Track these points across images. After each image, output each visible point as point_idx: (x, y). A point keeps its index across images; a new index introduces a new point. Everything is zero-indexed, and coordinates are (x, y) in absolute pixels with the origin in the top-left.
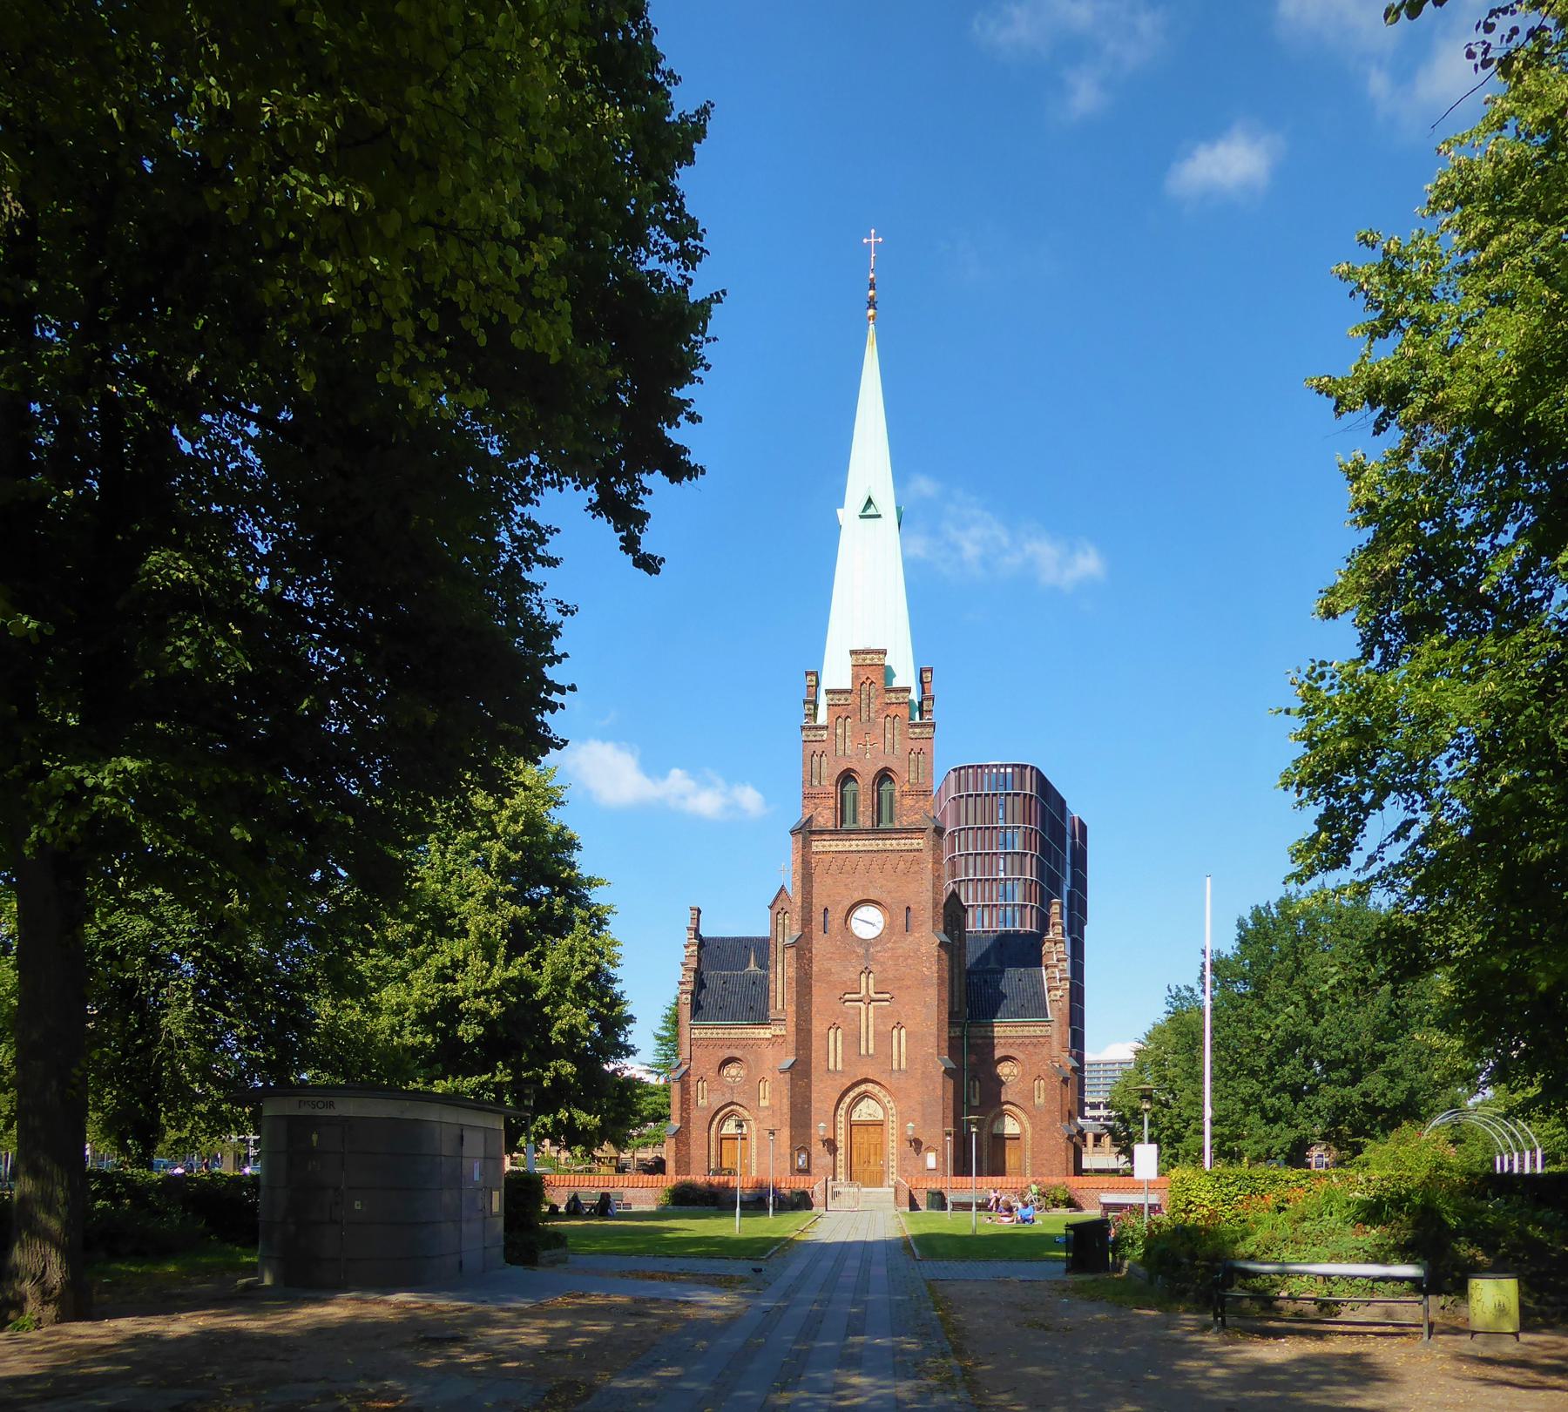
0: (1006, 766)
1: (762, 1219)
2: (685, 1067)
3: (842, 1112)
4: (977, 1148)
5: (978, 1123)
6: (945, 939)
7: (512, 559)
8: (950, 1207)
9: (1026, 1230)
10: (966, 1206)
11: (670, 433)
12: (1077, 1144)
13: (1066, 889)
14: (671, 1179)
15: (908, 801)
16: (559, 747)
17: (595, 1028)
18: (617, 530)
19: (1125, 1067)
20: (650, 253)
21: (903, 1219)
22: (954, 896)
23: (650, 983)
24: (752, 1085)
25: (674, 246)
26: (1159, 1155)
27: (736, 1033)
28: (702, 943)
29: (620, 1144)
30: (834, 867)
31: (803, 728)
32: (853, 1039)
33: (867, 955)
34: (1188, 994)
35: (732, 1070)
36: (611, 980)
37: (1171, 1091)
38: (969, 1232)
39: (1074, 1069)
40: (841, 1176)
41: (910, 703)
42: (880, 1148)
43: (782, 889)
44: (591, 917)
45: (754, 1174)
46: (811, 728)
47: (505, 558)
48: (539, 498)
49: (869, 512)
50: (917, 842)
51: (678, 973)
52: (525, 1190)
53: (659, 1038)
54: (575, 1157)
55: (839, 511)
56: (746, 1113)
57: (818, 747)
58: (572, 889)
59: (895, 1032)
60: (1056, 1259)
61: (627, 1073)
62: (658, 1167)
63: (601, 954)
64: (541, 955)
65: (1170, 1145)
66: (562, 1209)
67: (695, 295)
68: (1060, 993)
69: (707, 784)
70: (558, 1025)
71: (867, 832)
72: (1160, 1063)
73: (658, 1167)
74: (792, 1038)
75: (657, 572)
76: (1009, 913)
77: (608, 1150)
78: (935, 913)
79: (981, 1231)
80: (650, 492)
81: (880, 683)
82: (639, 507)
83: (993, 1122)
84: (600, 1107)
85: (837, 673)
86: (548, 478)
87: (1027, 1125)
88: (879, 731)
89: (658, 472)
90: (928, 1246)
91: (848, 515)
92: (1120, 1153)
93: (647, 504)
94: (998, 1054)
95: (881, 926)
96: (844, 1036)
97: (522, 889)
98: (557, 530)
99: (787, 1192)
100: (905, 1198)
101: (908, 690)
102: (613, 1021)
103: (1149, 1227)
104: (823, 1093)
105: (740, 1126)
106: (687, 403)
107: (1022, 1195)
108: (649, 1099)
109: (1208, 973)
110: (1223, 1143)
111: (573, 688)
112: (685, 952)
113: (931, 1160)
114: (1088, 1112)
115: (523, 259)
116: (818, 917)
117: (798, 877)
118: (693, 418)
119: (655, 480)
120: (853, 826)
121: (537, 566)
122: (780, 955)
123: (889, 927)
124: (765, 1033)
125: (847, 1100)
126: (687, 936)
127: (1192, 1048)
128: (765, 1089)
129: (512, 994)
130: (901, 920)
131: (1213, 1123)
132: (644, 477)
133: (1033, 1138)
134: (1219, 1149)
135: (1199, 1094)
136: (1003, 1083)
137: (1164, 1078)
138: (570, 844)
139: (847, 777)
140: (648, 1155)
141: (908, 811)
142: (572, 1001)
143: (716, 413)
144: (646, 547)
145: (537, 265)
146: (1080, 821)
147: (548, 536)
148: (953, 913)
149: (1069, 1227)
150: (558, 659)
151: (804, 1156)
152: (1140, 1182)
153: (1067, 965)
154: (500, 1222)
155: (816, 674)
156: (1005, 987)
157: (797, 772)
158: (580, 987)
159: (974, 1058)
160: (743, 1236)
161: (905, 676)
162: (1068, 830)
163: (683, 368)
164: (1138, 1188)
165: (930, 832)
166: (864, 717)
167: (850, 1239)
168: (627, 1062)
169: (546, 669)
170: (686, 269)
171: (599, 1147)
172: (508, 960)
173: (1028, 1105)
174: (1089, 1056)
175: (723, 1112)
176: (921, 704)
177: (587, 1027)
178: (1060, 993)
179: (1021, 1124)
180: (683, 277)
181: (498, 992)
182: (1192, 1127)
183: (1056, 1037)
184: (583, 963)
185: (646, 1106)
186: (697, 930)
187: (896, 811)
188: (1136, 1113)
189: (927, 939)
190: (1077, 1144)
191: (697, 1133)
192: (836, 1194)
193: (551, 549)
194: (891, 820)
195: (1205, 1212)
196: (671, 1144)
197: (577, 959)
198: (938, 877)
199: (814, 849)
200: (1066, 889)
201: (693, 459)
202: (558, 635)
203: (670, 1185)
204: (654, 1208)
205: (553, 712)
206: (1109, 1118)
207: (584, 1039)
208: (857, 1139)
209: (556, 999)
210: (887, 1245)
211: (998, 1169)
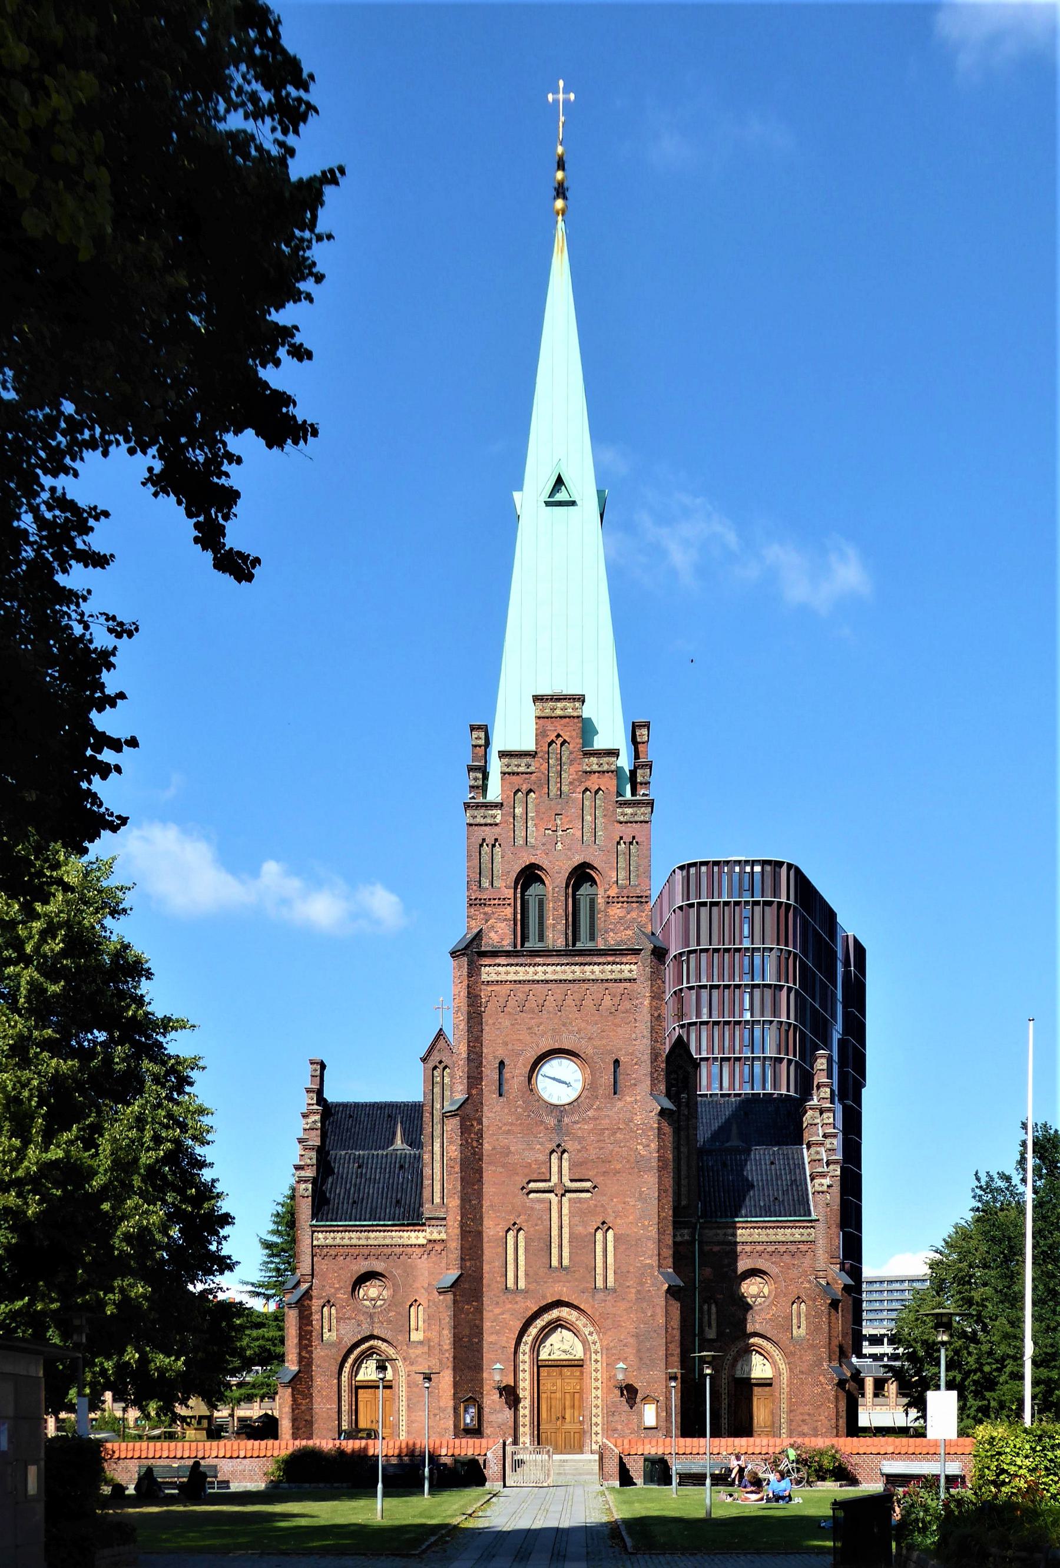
0: (753, 863)
1: (414, 1500)
2: (304, 1286)
3: (525, 1348)
4: (715, 1401)
5: (713, 1362)
6: (668, 1104)
7: (39, 554)
8: (675, 1480)
9: (781, 1510)
10: (697, 1479)
11: (268, 374)
12: (850, 1392)
13: (836, 1035)
14: (286, 1445)
15: (616, 911)
16: (115, 829)
17: (175, 1232)
18: (190, 515)
19: (918, 1285)
20: (232, 106)
21: (611, 1498)
22: (680, 1046)
23: (254, 1170)
24: (400, 1311)
25: (266, 97)
26: (962, 1409)
27: (376, 1238)
28: (328, 1111)
29: (213, 1396)
30: (512, 1003)
31: (467, 806)
32: (541, 1246)
33: (559, 1128)
34: (1002, 1184)
35: (372, 1290)
36: (202, 1165)
37: (979, 1319)
38: (701, 1514)
39: (846, 1288)
40: (525, 1439)
41: (618, 771)
42: (578, 1399)
43: (440, 1034)
44: (168, 1073)
45: (403, 1436)
46: (478, 806)
47: (28, 553)
48: (77, 465)
49: (562, 496)
50: (628, 969)
51: (294, 1153)
52: (81, 1458)
53: (267, 1245)
54: (147, 1417)
55: (517, 495)
56: (391, 1351)
57: (489, 834)
58: (143, 1033)
59: (599, 1235)
60: (822, 1550)
61: (221, 1296)
62: (267, 1428)
63: (184, 1127)
64: (97, 1129)
65: (977, 1394)
66: (131, 1490)
67: (299, 170)
68: (827, 1181)
69: (315, 883)
70: (124, 1227)
71: (559, 953)
72: (964, 1280)
73: (267, 1428)
74: (455, 1245)
75: (250, 578)
76: (758, 1069)
77: (196, 1406)
78: (654, 1069)
79: (718, 1513)
80: (239, 461)
81: (575, 744)
82: (223, 481)
83: (735, 1361)
84: (183, 1343)
85: (515, 728)
86: (87, 434)
87: (783, 1366)
88: (574, 811)
89: (249, 432)
90: (641, 1533)
91: (529, 499)
92: (909, 1405)
93: (235, 477)
94: (743, 1265)
95: (578, 1086)
96: (527, 1240)
97: (67, 1036)
98: (106, 514)
99: (445, 1460)
100: (613, 1468)
101: (614, 753)
102: (203, 1220)
103: (946, 1506)
104: (499, 1322)
105: (381, 1368)
106: (287, 332)
107: (776, 1463)
108: (255, 1333)
109: (1030, 1155)
110: (1050, 1392)
111: (133, 743)
112: (302, 1123)
113: (650, 1415)
114: (867, 1349)
115: (35, 102)
116: (490, 1073)
117: (463, 1017)
118: (301, 353)
119: (245, 443)
120: (539, 946)
121: (77, 567)
122: (438, 1128)
123: (591, 1087)
124: (416, 1237)
125: (533, 1331)
126: (306, 1101)
127: (1007, 1260)
128: (418, 1317)
129: (57, 1185)
130: (607, 1078)
131: (1034, 1363)
132: (229, 438)
133: (790, 1383)
134: (1045, 1399)
135: (1017, 1323)
136: (749, 1307)
137: (969, 1302)
138: (137, 969)
139: (530, 876)
140: (253, 1411)
141: (617, 925)
142: (142, 1194)
143: (332, 342)
144: (236, 536)
145: (56, 112)
146: (856, 940)
147: (91, 522)
148: (678, 1069)
149: (837, 1505)
150: (111, 701)
151: (472, 1410)
152: (936, 1443)
153: (837, 1143)
154: (40, 1508)
155: (485, 729)
156: (751, 1172)
157: (459, 870)
158: (152, 1172)
159: (708, 1271)
160: (387, 1522)
161: (611, 734)
162: (840, 954)
163: (289, 277)
164: (930, 1455)
165: (646, 954)
166: (554, 791)
167: (538, 1525)
168: (225, 1280)
169: (94, 715)
170: (285, 132)
171: (184, 1402)
172: (49, 1137)
173: (783, 1338)
174: (869, 1270)
175: (361, 1348)
176: (633, 773)
177: (164, 1229)
178: (827, 1181)
179: (774, 1364)
180: (281, 144)
181: (36, 1182)
182: (1008, 1370)
183: (821, 1242)
184: (157, 1140)
185: (249, 1342)
186: (320, 1092)
187: (600, 924)
188: (932, 1348)
189: (643, 1105)
190: (850, 1392)
191: (322, 1382)
192: (518, 1464)
193: (98, 540)
194: (592, 938)
195: (1023, 1485)
196: (285, 1396)
197: (148, 1134)
198: (657, 1019)
199: (484, 977)
200: (836, 1035)
201: (301, 413)
202: (110, 666)
203: (285, 1453)
204: (262, 1486)
205: (104, 777)
206: (895, 1357)
207: (160, 1248)
208: (546, 1385)
209: (118, 1190)
210: (588, 1532)
211: (743, 1427)
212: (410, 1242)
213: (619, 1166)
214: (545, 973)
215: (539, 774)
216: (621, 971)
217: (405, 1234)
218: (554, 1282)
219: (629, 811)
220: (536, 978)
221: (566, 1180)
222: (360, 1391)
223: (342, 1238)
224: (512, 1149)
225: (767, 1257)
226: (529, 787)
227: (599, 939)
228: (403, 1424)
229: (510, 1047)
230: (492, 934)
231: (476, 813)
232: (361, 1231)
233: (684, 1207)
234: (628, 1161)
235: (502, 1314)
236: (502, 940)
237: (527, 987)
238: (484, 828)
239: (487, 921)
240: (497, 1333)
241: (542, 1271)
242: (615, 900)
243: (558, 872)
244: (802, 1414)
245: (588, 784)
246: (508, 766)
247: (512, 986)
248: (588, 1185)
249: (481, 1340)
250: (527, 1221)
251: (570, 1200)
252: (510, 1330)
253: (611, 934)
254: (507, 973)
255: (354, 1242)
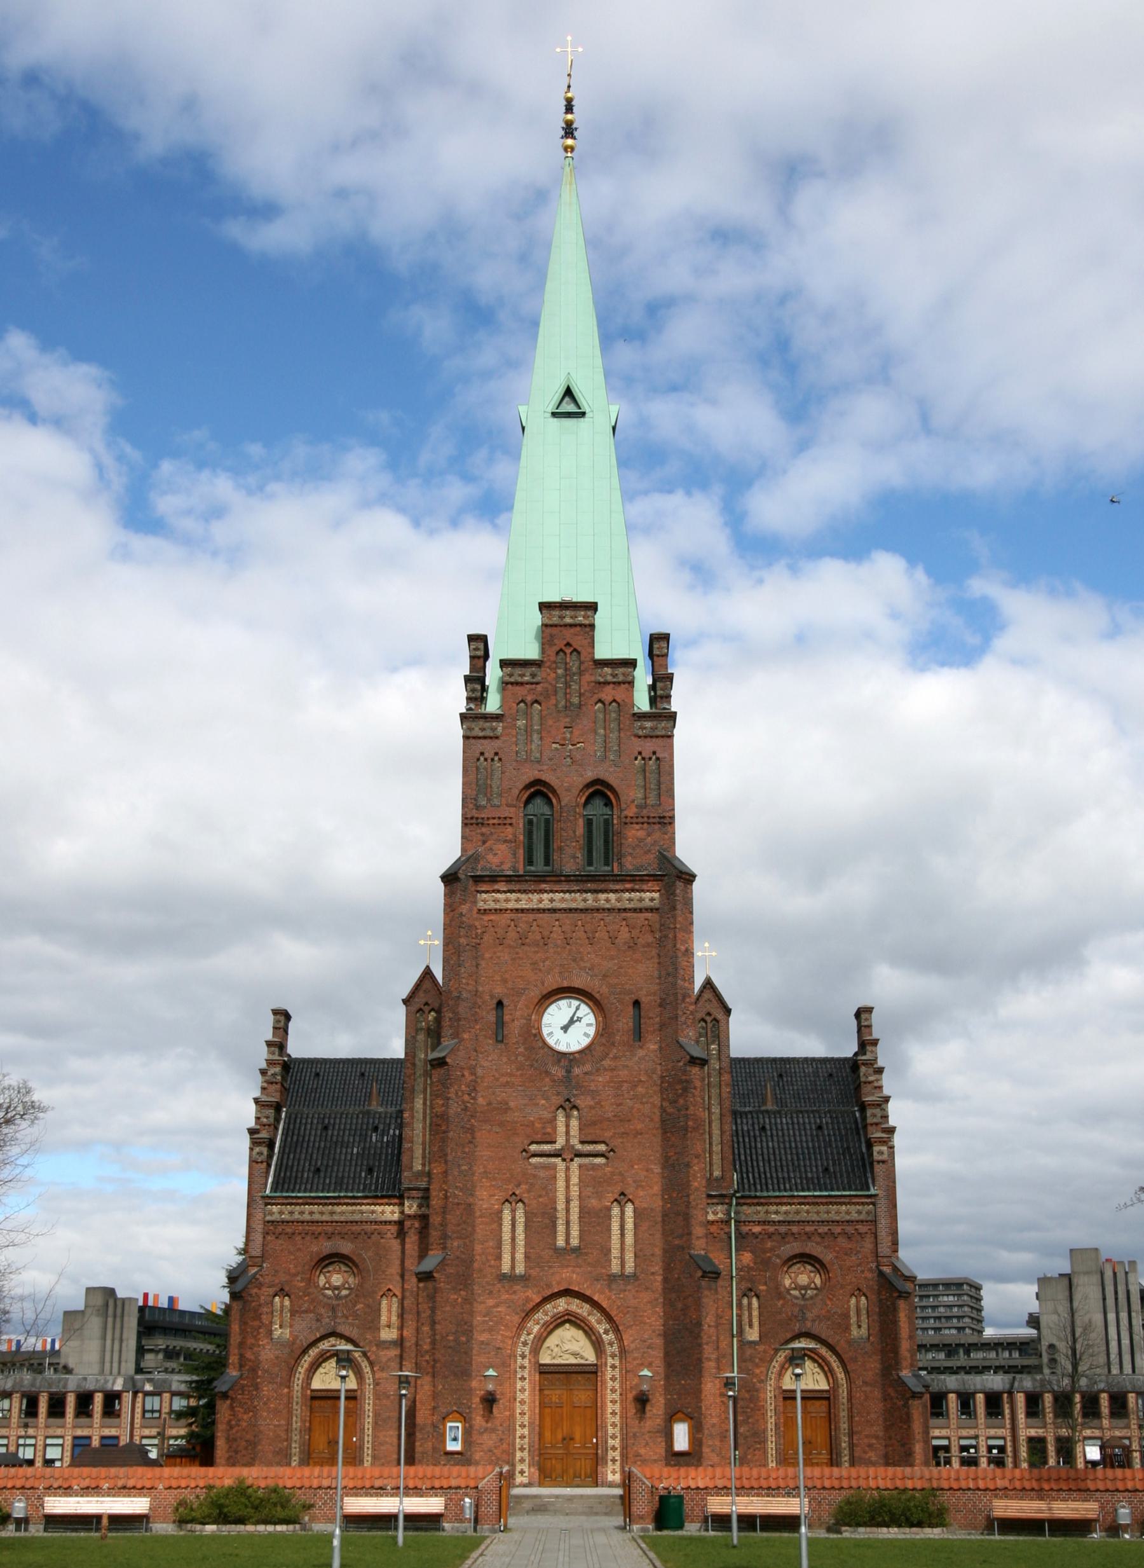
27: (343, 1212)
30: (512, 934)
32: (542, 1223)
33: (568, 1080)
49: (569, 407)
57: (489, 747)
87: (841, 1375)
123: (604, 1032)
212: (383, 1218)
213: (639, 1126)
214: (552, 900)
215: (546, 685)
216: (641, 900)
217: (379, 1208)
218: (563, 1266)
219: (648, 724)
220: (541, 906)
221: (574, 1141)
222: (825, 1403)
223: (302, 1213)
224: (512, 1104)
225: (819, 1239)
226: (534, 697)
227: (615, 865)
228: (368, 1445)
229: (510, 985)
230: (490, 857)
231: (473, 725)
232: (326, 1204)
233: (717, 1179)
234: (652, 1120)
235: (497, 1306)
236: (502, 863)
237: (531, 916)
238: (482, 741)
239: (484, 842)
240: (490, 1330)
241: (547, 1254)
242: (635, 820)
243: (569, 783)
244: (867, 1436)
245: (603, 696)
246: (511, 675)
247: (513, 916)
248: (602, 1148)
249: (470, 1338)
250: (529, 1191)
251: (580, 1166)
252: (506, 1326)
253: (629, 858)
254: (507, 900)
255: (317, 1217)
